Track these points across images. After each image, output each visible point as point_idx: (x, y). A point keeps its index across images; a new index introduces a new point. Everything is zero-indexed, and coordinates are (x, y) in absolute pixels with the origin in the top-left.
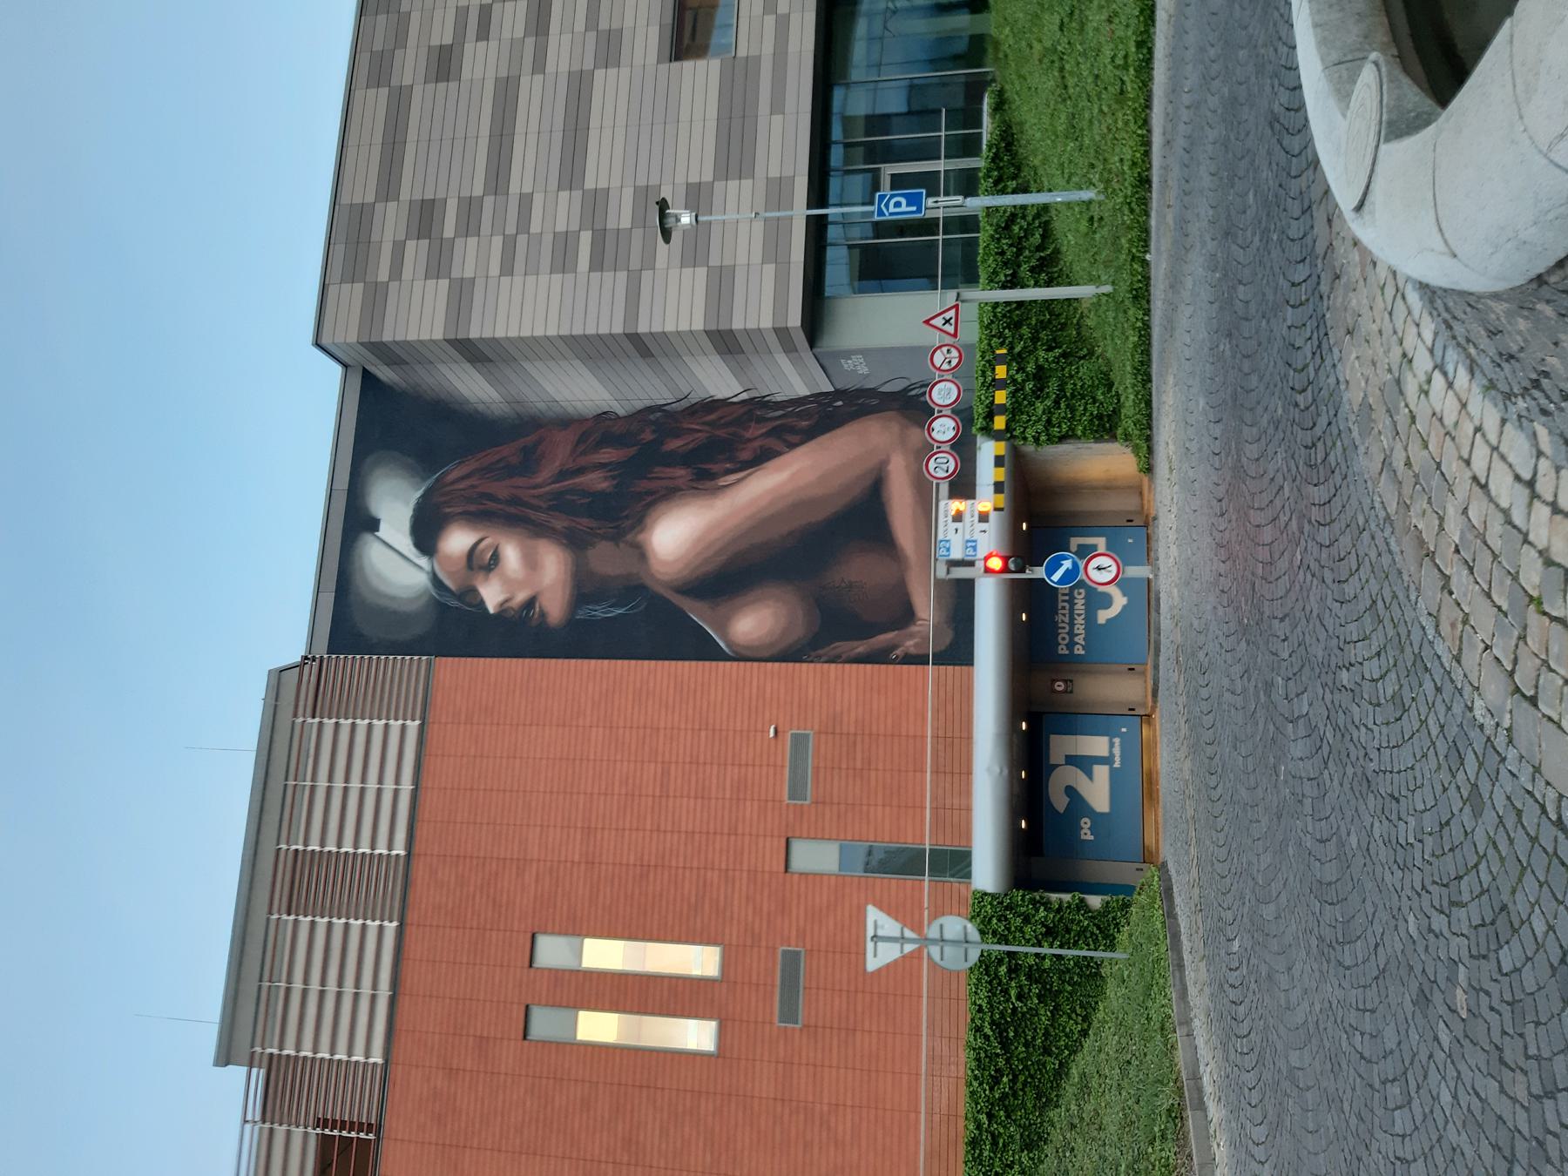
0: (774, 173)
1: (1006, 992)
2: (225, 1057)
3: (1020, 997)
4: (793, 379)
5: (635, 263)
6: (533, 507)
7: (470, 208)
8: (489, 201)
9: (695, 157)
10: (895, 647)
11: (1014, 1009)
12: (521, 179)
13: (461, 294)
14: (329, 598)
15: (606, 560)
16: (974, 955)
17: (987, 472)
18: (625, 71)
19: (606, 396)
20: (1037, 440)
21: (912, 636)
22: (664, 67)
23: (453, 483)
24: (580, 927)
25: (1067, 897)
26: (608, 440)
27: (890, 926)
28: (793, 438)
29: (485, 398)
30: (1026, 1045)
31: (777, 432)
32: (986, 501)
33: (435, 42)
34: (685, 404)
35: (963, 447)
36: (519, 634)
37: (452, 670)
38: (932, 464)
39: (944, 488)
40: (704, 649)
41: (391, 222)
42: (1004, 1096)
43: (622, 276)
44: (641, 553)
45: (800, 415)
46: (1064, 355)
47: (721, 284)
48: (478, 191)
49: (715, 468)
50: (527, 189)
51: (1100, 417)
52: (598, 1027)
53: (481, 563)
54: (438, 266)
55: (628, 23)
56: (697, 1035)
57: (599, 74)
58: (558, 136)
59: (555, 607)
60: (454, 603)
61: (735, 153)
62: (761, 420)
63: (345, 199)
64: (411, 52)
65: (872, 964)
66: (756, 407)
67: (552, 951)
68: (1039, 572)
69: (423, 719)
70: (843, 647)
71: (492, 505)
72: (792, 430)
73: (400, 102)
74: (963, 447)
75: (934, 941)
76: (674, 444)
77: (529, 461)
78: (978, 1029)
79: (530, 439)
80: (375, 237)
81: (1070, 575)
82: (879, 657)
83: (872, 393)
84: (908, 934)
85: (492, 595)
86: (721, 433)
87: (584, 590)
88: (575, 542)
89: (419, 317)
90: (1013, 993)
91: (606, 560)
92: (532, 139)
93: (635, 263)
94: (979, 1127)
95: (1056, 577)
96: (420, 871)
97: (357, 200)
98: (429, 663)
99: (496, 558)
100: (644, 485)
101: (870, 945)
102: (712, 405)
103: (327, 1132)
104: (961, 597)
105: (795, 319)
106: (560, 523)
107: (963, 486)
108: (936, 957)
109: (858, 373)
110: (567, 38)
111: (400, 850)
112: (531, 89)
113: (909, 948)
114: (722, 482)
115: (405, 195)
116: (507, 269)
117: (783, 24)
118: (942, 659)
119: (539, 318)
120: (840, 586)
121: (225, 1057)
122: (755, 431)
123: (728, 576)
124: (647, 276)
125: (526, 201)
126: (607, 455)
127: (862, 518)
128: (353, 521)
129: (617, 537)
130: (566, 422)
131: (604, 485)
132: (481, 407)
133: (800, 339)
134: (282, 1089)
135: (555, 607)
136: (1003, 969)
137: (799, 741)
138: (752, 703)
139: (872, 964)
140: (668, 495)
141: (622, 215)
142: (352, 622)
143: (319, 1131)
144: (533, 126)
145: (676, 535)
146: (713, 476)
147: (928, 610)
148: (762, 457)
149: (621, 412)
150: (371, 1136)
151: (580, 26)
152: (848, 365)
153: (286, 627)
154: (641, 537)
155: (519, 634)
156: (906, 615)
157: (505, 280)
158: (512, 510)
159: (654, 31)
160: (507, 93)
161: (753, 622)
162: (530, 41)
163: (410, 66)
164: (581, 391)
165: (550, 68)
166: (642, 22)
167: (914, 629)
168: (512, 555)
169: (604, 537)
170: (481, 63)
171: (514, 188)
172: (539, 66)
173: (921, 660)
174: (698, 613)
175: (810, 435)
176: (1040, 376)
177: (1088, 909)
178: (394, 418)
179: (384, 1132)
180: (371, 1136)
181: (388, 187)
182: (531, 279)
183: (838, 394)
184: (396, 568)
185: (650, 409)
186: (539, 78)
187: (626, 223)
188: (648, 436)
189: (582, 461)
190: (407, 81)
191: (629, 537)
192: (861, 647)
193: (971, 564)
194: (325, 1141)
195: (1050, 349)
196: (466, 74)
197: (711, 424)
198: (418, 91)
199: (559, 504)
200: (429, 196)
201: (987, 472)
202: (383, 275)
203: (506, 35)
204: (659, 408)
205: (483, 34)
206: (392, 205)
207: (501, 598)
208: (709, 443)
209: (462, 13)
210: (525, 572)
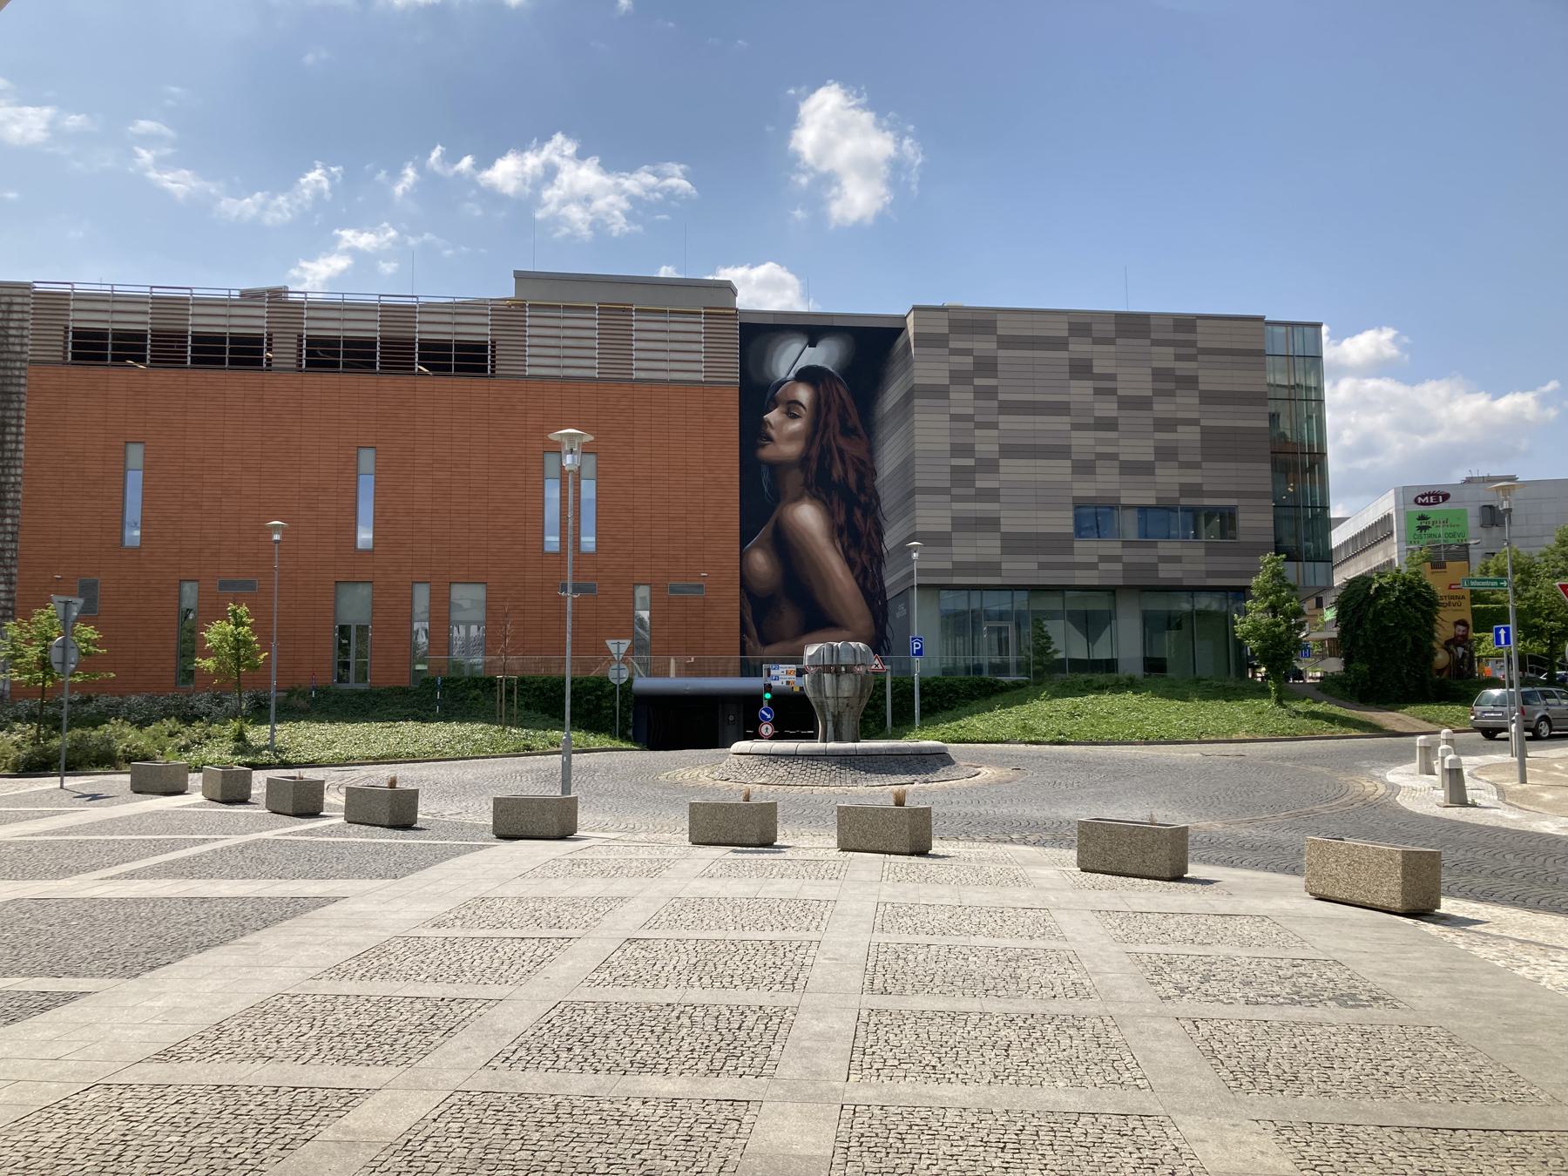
0: (1004, 566)
2: (520, 276)
5: (955, 491)
7: (990, 393)
9: (1015, 521)
12: (1007, 422)
13: (939, 392)
15: (794, 479)
18: (1002, 514)
22: (1070, 501)
26: (861, 478)
27: (623, 649)
31: (864, 570)
36: (752, 432)
37: (732, 397)
40: (746, 536)
41: (984, 345)
43: (948, 485)
44: (798, 499)
47: (935, 540)
48: (1001, 397)
49: (845, 538)
54: (958, 377)
56: (552, 541)
59: (767, 453)
61: (1016, 544)
63: (999, 316)
64: (1088, 348)
65: (609, 642)
70: (749, 610)
72: (865, 578)
73: (1058, 344)
76: (858, 514)
77: (848, 432)
79: (861, 432)
80: (977, 337)
81: (764, 717)
82: (744, 628)
83: (885, 620)
85: (773, 416)
87: (777, 468)
88: (803, 461)
89: (926, 369)
91: (794, 479)
92: (1030, 427)
93: (955, 491)
99: (795, 417)
100: (836, 499)
102: (880, 534)
106: (814, 452)
109: (896, 612)
110: (1092, 442)
111: (636, 375)
112: (1061, 423)
115: (1001, 353)
116: (955, 418)
119: (917, 440)
120: (784, 606)
121: (520, 276)
122: (865, 557)
123: (786, 546)
124: (948, 498)
125: (994, 426)
126: (852, 478)
127: (818, 620)
128: (812, 330)
129: (807, 485)
130: (871, 451)
131: (835, 475)
134: (508, 314)
135: (767, 453)
138: (719, 561)
139: (609, 642)
140: (830, 514)
141: (982, 482)
142: (760, 334)
144: (1038, 427)
145: (807, 516)
146: (840, 536)
148: (850, 562)
151: (1099, 449)
152: (901, 607)
155: (752, 432)
156: (766, 642)
159: (1093, 494)
160: (1060, 409)
161: (760, 561)
162: (1092, 421)
164: (888, 460)
168: (796, 426)
170: (1081, 391)
171: (1002, 418)
172: (1076, 427)
173: (743, 652)
174: (766, 531)
175: (863, 588)
178: (871, 347)
181: (1006, 342)
182: (947, 432)
183: (885, 603)
185: (878, 498)
186: (1068, 427)
187: (978, 484)
188: (863, 498)
189: (848, 462)
192: (749, 619)
198: (1065, 354)
199: (825, 452)
202: (952, 345)
203: (1097, 405)
205: (1098, 391)
206: (994, 346)
208: (859, 529)
210: (786, 433)
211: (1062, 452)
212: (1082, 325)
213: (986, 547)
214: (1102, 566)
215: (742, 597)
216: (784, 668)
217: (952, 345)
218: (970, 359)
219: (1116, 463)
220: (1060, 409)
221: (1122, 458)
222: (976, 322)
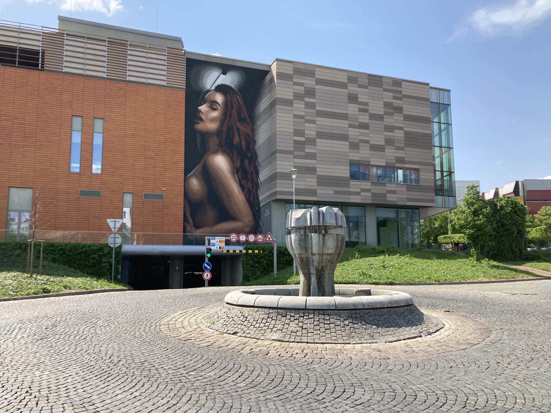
0: (318, 191)
1: (94, 254)
3: (93, 258)
4: (263, 196)
6: (229, 121)
8: (314, 111)
9: (323, 170)
10: (188, 223)
11: (89, 256)
12: (320, 121)
13: (288, 103)
14: (203, 59)
15: (214, 142)
16: (112, 246)
17: (231, 249)
19: (260, 143)
20: (243, 261)
21: (191, 228)
23: (237, 98)
24: (105, 131)
25: (120, 269)
28: (247, 196)
29: (261, 107)
30: (80, 259)
31: (249, 191)
32: (225, 249)
33: (359, 96)
34: (258, 165)
35: (238, 243)
37: (181, 96)
38: (234, 235)
39: (228, 238)
40: (187, 170)
41: (310, 82)
42: (65, 253)
44: (216, 152)
45: (254, 198)
46: (265, 268)
48: (317, 108)
49: (240, 174)
50: (317, 122)
51: (248, 277)
52: (77, 138)
53: (213, 105)
55: (361, 151)
56: (75, 167)
57: (347, 143)
58: (331, 131)
59: (200, 126)
60: (201, 97)
61: (324, 181)
62: (253, 187)
63: (317, 69)
65: (109, 221)
66: (256, 185)
67: (99, 125)
68: (207, 261)
69: (167, 86)
70: (188, 209)
71: (229, 109)
72: (249, 196)
73: (343, 85)
74: (238, 243)
75: (115, 236)
76: (246, 162)
77: (242, 120)
78: (84, 247)
81: (206, 268)
83: (259, 217)
84: (116, 230)
85: (203, 108)
86: (249, 176)
87: (205, 135)
88: (219, 132)
89: (283, 90)
90: (94, 256)
91: (214, 142)
93: (295, 153)
94: (57, 246)
95: (206, 265)
96: (122, 85)
97: (316, 73)
98: (184, 89)
99: (214, 109)
100: (235, 154)
101: (113, 220)
102: (257, 173)
103: (41, 54)
104: (201, 242)
105: (279, 197)
106: (225, 129)
107: (228, 243)
108: (111, 236)
109: (266, 213)
112: (344, 124)
113: (113, 230)
114: (236, 175)
115: (317, 87)
116: (296, 116)
117: (358, 194)
118: (185, 237)
121: (62, 19)
122: (250, 185)
123: (209, 177)
124: (292, 156)
125: (314, 122)
126: (244, 143)
128: (225, 67)
129: (220, 145)
130: (253, 131)
131: (235, 142)
132: (258, 106)
133: (274, 198)
134: (55, 39)
135: (200, 126)
136: (101, 253)
137: (161, 197)
138: (172, 180)
139: (109, 221)
142: (196, 65)
143: (41, 51)
145: (221, 162)
146: (237, 173)
147: (198, 233)
148: (242, 187)
149: (256, 147)
150: (40, 67)
151: (361, 138)
152: (267, 211)
153: (194, 46)
154: (220, 152)
155: (192, 117)
156: (197, 227)
157: (292, 116)
158: (228, 115)
159: (358, 159)
160: (344, 117)
161: (195, 183)
162: (358, 124)
163: (353, 88)
164: (262, 135)
165: (350, 129)
166: (361, 155)
167: (193, 229)
168: (215, 114)
169: (220, 141)
170: (353, 109)
171: (317, 119)
172: (351, 126)
173: (185, 231)
174: (198, 168)
175: (248, 200)
176: (258, 262)
177: (117, 275)
178: (254, 79)
179: (42, 72)
180: (40, 67)
182: (292, 123)
184: (212, 79)
186: (347, 126)
187: (307, 150)
188: (249, 155)
190: (349, 88)
191: (220, 149)
192: (188, 214)
193: (209, 245)
194: (37, 53)
195: (266, 264)
196: (350, 105)
197: (252, 173)
198: (346, 91)
199: (230, 129)
200: (316, 94)
201: (231, 249)
202: (295, 80)
203: (360, 117)
204: (257, 158)
205: (360, 110)
207: (203, 111)
209: (366, 104)
210: (210, 118)
211: (344, 137)
212: (354, 78)
213: (311, 182)
214: (362, 194)
215: (185, 202)
216: (218, 239)
217: (295, 80)
218: (303, 88)
219: (368, 145)
220: (344, 117)
221: (371, 142)
222: (306, 70)
